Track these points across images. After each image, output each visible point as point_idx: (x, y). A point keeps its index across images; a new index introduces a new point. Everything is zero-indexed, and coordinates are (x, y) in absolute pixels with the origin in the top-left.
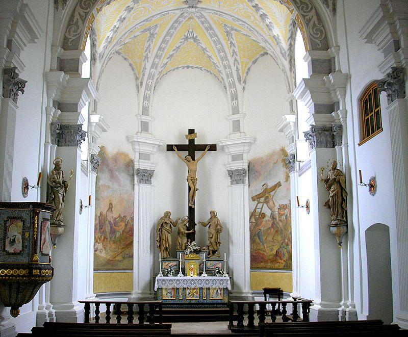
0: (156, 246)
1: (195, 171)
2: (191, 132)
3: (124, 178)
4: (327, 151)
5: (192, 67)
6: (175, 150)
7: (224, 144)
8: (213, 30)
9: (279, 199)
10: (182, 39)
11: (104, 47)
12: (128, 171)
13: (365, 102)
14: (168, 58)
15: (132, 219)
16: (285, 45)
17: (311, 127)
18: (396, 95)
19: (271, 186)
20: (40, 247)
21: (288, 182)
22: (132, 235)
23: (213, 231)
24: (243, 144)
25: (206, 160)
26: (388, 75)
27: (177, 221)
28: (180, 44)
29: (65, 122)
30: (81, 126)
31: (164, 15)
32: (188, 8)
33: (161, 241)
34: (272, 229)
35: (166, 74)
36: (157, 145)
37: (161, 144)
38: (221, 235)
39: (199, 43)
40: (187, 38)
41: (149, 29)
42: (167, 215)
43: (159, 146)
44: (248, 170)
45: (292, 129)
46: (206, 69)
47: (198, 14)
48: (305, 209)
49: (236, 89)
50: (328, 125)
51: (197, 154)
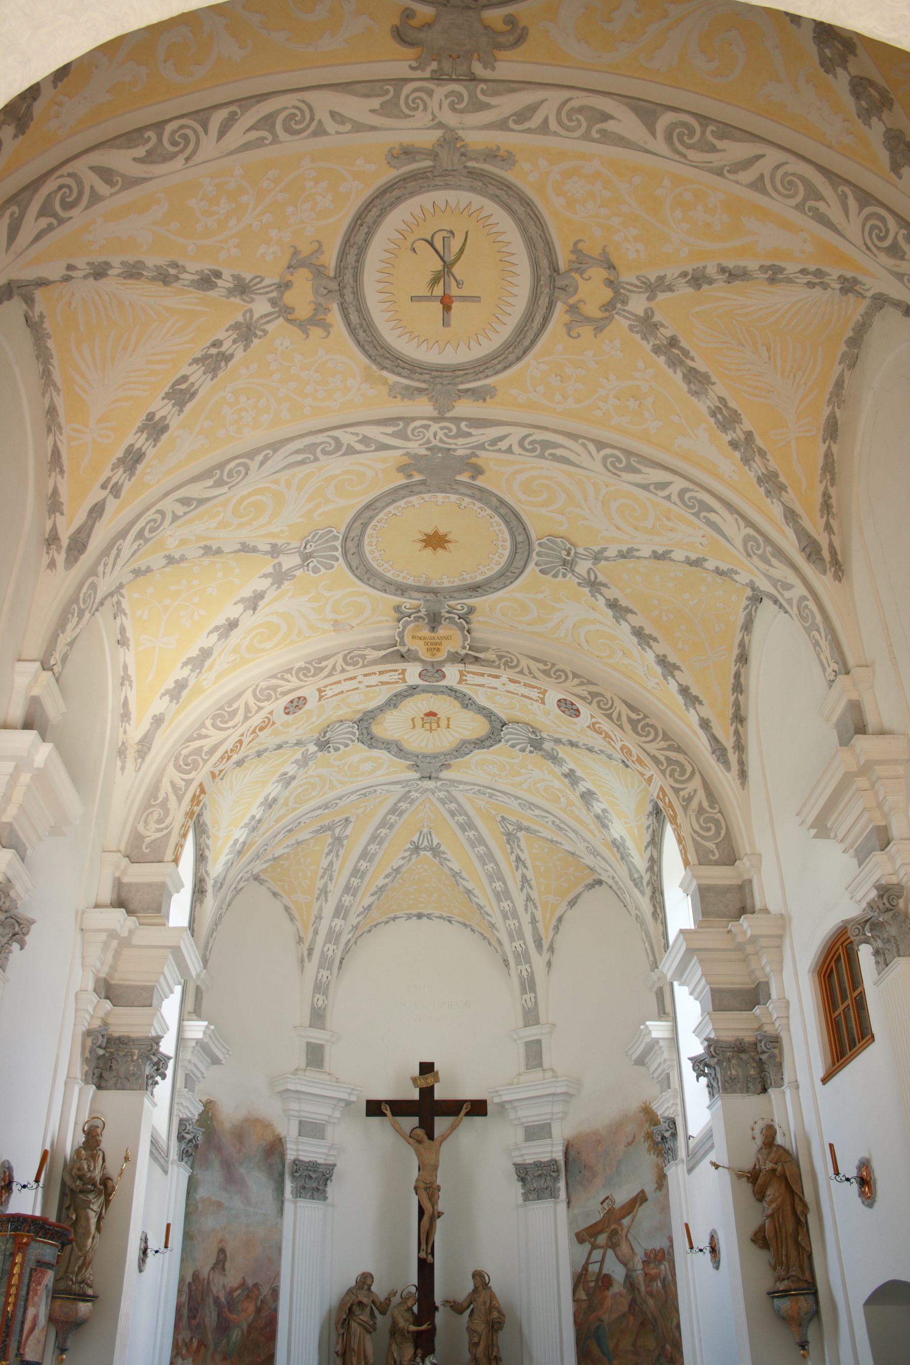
1: (436, 1167)
2: (427, 1068)
3: (257, 1182)
4: (749, 1105)
5: (429, 916)
6: (385, 1115)
7: (505, 1098)
8: (476, 830)
9: (641, 1236)
10: (405, 851)
11: (226, 863)
13: (829, 976)
14: (373, 895)
15: (275, 1293)
16: (640, 862)
17: (706, 1043)
18: (895, 950)
19: (622, 1204)
20: (20, 1342)
21: (664, 1191)
23: (481, 1327)
24: (550, 1098)
25: (464, 1140)
26: (870, 906)
27: (388, 1300)
28: (401, 862)
29: (117, 1031)
30: (157, 1040)
31: (365, 795)
32: (420, 779)
34: (631, 1319)
35: (370, 931)
36: (340, 1100)
38: (503, 1337)
39: (446, 859)
40: (416, 849)
41: (330, 828)
42: (365, 1281)
43: (348, 1103)
45: (666, 1055)
46: (462, 920)
47: (442, 794)
48: (708, 1255)
49: (531, 967)
50: (748, 1037)
51: (441, 1124)
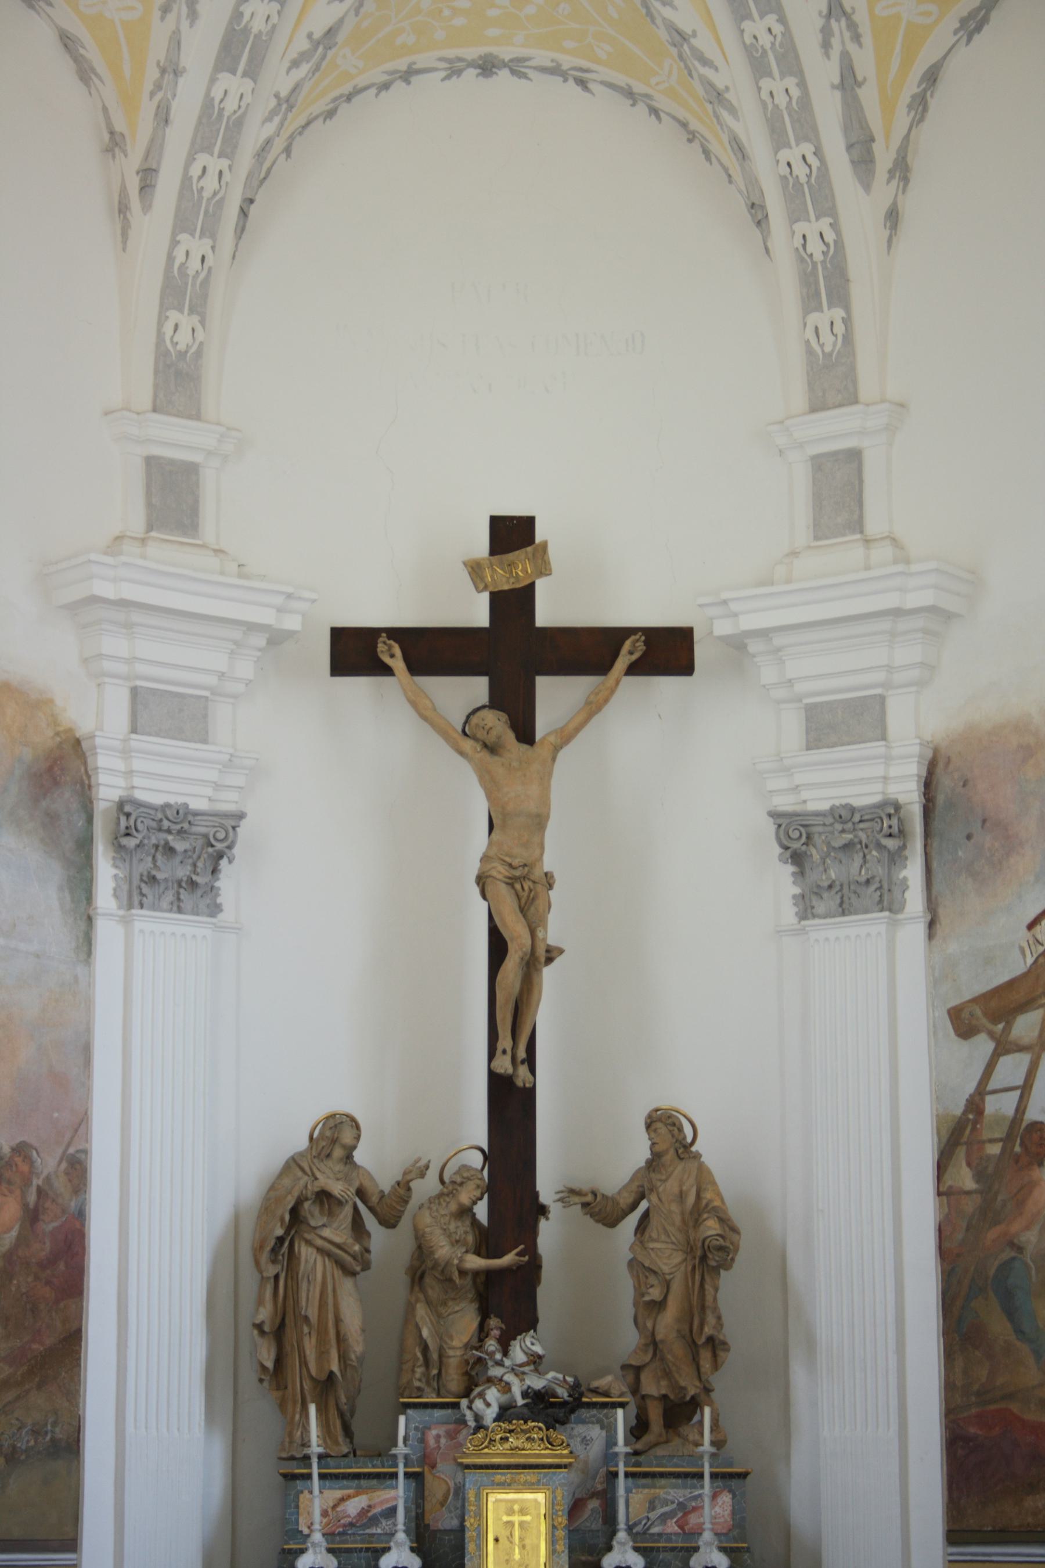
0: (249, 1375)
2: (512, 534)
5: (517, 68)
7: (748, 623)
12: (51, 819)
15: (77, 1169)
22: (73, 1286)
23: (669, 1259)
25: (618, 746)
27: (403, 1188)
33: (290, 1334)
35: (330, 114)
36: (251, 627)
37: (292, 623)
38: (731, 1290)
42: (335, 1136)
43: (277, 638)
44: (928, 812)
46: (621, 79)
51: (555, 697)
